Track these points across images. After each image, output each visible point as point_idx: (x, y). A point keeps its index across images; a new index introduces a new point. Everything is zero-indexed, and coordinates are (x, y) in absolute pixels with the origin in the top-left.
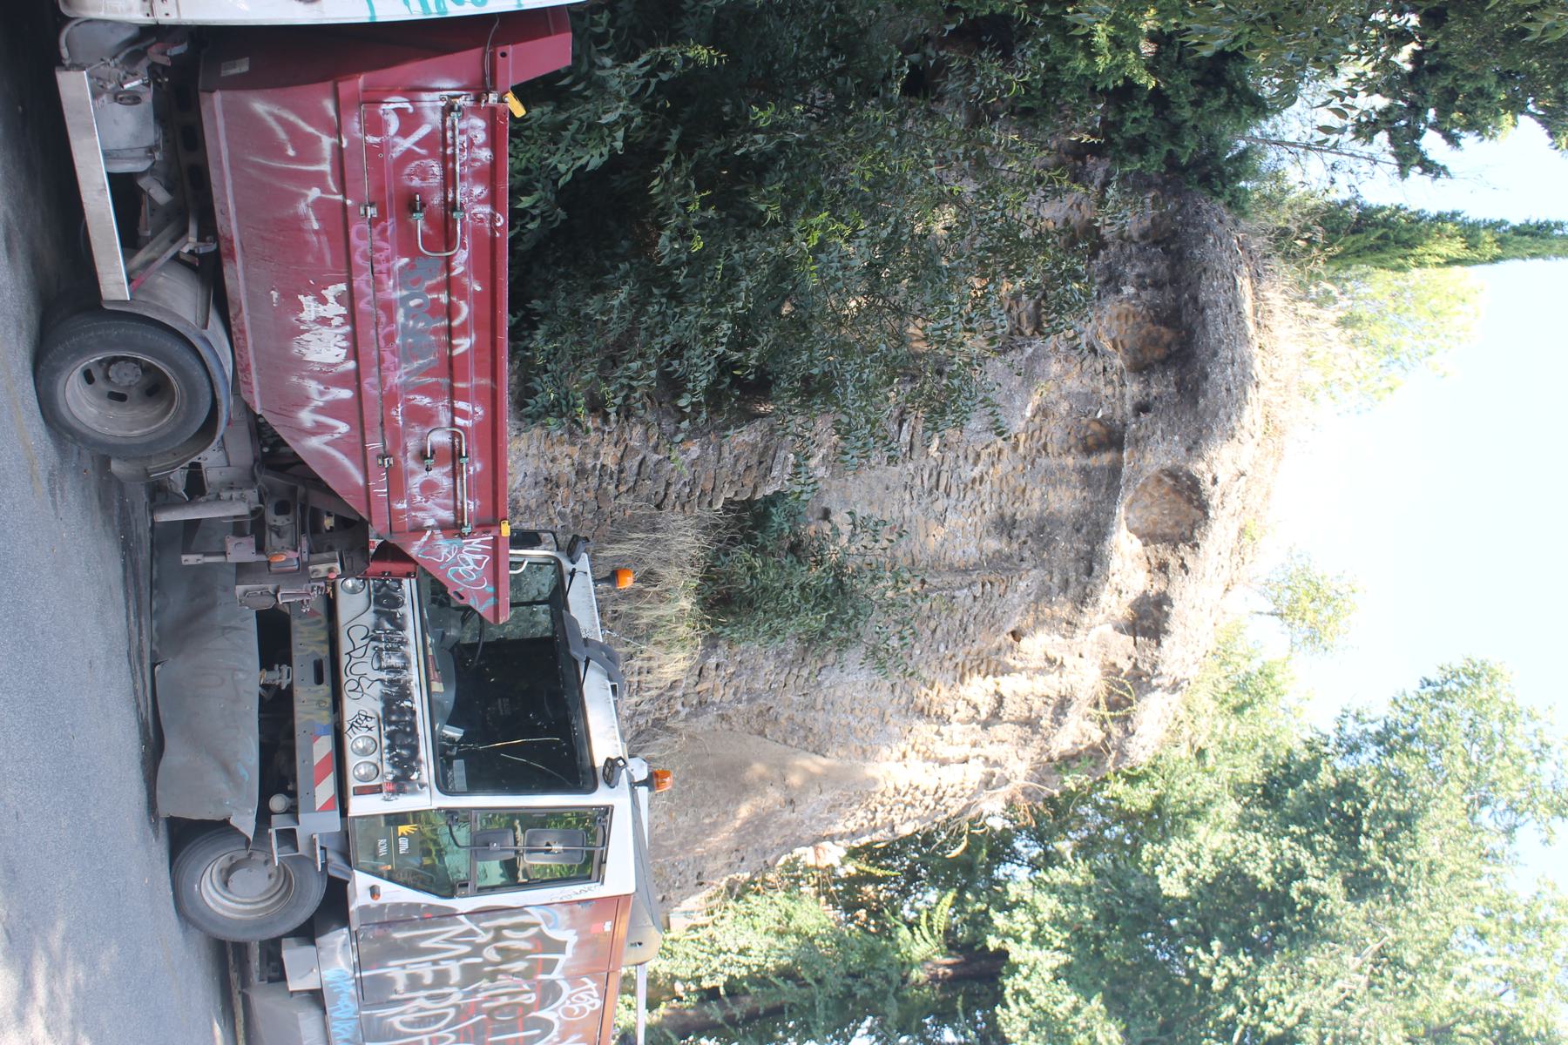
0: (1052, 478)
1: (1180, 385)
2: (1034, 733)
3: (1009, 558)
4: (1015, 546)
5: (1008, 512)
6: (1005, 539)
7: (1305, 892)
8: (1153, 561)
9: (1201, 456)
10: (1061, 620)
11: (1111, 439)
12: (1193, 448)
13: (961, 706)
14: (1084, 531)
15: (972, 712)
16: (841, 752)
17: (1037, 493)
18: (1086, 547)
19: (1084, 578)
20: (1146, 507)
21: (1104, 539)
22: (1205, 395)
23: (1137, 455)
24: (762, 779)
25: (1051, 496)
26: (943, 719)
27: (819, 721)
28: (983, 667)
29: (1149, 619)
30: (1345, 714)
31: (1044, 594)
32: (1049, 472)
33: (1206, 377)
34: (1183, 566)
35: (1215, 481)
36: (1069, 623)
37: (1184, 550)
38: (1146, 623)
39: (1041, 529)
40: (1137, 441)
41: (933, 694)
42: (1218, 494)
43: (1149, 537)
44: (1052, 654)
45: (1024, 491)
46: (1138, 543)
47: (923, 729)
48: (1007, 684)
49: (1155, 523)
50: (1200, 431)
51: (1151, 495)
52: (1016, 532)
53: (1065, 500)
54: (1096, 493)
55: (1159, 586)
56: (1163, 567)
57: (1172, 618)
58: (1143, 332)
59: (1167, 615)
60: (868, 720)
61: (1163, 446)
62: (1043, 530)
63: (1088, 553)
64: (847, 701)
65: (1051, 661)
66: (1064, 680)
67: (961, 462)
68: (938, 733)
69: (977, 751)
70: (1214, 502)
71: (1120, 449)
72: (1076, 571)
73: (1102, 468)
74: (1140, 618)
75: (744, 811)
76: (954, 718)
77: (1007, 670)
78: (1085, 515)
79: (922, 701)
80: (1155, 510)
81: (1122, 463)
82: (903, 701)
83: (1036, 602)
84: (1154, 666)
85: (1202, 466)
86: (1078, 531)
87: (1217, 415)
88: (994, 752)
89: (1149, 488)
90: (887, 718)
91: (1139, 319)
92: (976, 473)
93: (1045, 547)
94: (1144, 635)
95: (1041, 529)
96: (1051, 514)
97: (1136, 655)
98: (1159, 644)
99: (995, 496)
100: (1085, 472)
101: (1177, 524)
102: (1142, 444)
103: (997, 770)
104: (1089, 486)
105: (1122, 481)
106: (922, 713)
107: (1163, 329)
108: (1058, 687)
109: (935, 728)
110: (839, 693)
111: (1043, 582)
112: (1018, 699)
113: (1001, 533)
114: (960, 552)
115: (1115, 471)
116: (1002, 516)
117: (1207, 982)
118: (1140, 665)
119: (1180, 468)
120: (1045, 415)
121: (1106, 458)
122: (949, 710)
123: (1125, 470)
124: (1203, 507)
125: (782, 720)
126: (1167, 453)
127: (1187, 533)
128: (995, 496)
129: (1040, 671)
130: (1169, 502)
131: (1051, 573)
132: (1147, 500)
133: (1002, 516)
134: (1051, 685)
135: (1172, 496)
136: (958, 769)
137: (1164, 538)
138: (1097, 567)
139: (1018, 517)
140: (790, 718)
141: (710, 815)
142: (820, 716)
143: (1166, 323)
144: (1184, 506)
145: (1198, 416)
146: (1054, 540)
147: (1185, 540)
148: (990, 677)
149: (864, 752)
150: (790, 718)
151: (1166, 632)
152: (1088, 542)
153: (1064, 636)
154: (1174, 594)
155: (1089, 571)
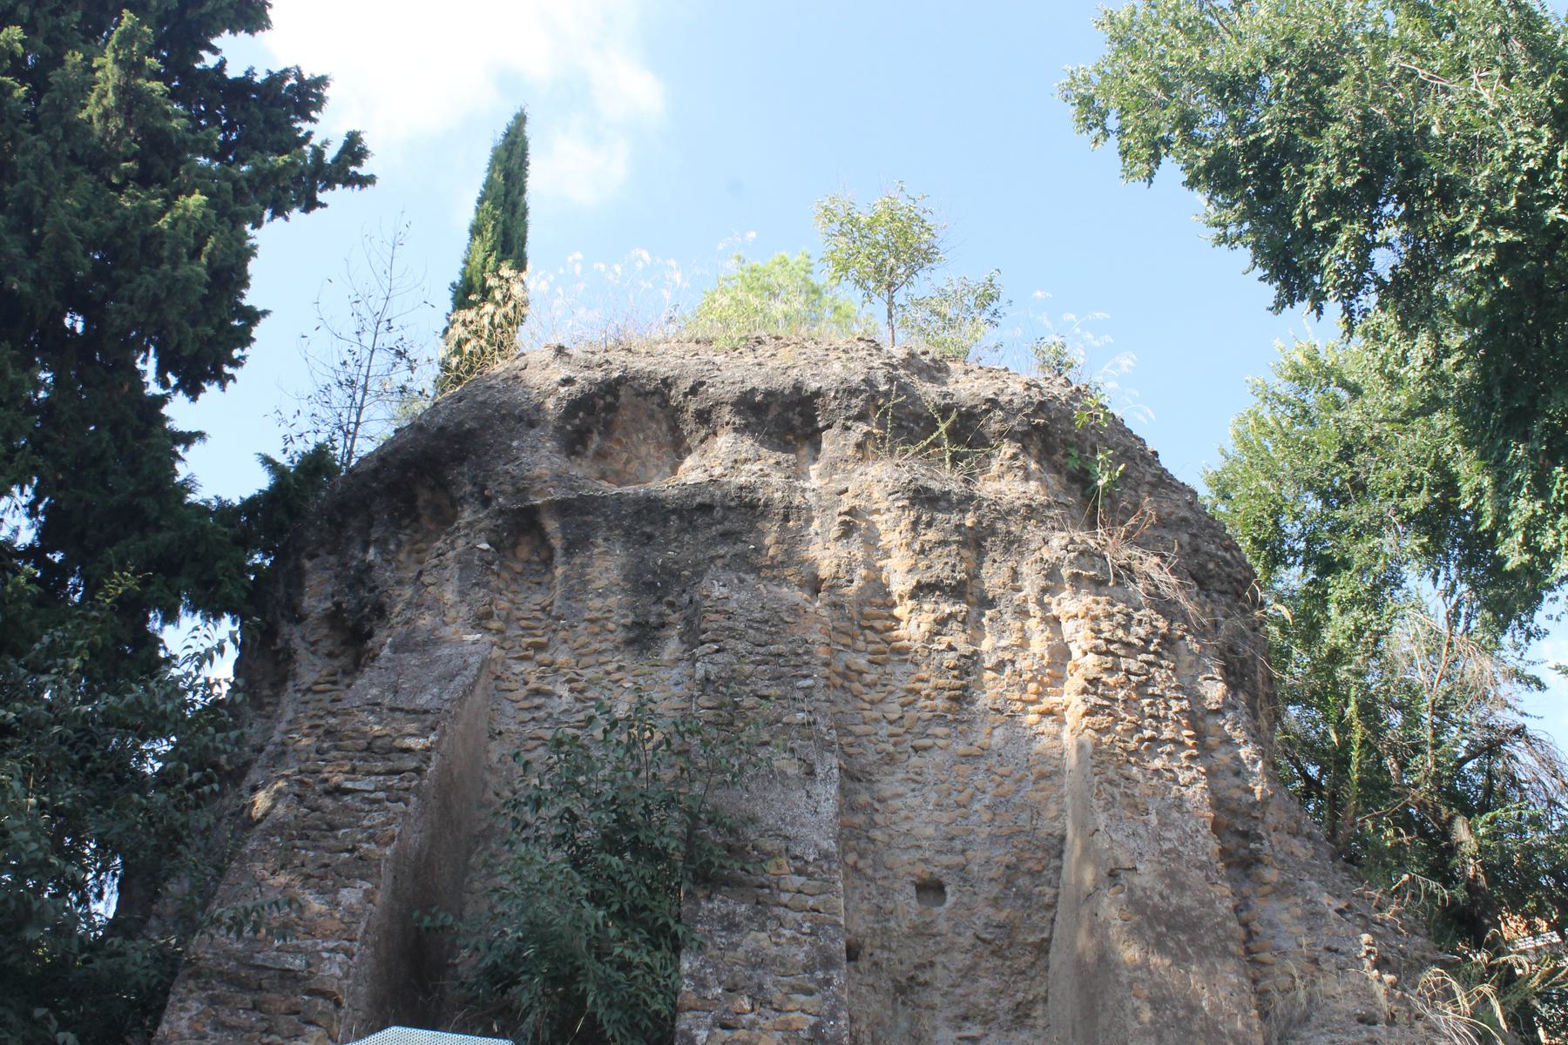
0: (578, 588)
1: (460, 459)
2: (994, 533)
3: (688, 621)
4: (674, 617)
5: (621, 635)
6: (664, 633)
7: (1344, 171)
8: (703, 433)
9: (539, 408)
10: (783, 529)
11: (522, 524)
12: (529, 418)
13: (941, 643)
14: (648, 529)
15: (954, 625)
16: (1052, 810)
17: (598, 603)
18: (674, 521)
19: (718, 513)
20: (643, 464)
21: (656, 500)
22: (461, 424)
23: (538, 486)
24: (1091, 932)
25: (600, 584)
26: (969, 665)
27: (986, 857)
28: (878, 624)
29: (787, 419)
30: (1223, 239)
31: (748, 564)
32: (569, 595)
33: (442, 429)
34: (694, 391)
35: (568, 381)
36: (786, 518)
37: (676, 395)
38: (797, 421)
39: (650, 586)
40: (519, 491)
41: (926, 689)
42: (587, 373)
43: (679, 449)
44: (835, 531)
45: (592, 621)
46: (689, 461)
47: (992, 688)
48: (899, 582)
49: (659, 446)
50: (503, 417)
51: (628, 462)
52: (653, 619)
53: (607, 565)
54: (595, 527)
55: (726, 414)
56: (703, 417)
57: (774, 385)
58: (432, 527)
59: (769, 394)
60: (979, 779)
61: (526, 457)
62: (650, 584)
63: (681, 518)
64: (945, 817)
65: (847, 530)
66: (883, 506)
67: (542, 714)
68: (999, 667)
69: (1032, 608)
70: (598, 375)
71: (533, 511)
72: (709, 526)
73: (563, 527)
74: (792, 429)
75: (1131, 953)
76: (965, 649)
77: (878, 589)
78: (628, 533)
79: (940, 703)
80: (643, 450)
81: (550, 503)
82: (941, 731)
83: (756, 569)
84: (852, 392)
85: (550, 404)
86: (650, 537)
87: (484, 403)
88: (1031, 582)
89: (618, 466)
90: (974, 750)
91: (418, 536)
92: (563, 691)
93: (675, 575)
94: (814, 419)
95: (650, 586)
96: (626, 578)
97: (840, 421)
98: (818, 394)
99: (602, 659)
100: (569, 550)
101: (651, 417)
102: (523, 484)
103: (1066, 572)
104: (587, 537)
105: (572, 495)
106: (962, 697)
107: (420, 503)
108: (895, 513)
109: (989, 675)
110: (930, 831)
111: (725, 567)
112: (922, 565)
113: (654, 639)
114: (676, 690)
115: (563, 509)
116: (629, 643)
117: (1505, 251)
118: (855, 412)
119: (558, 429)
120: (489, 615)
121: (551, 525)
122: (950, 659)
123: (558, 495)
124: (611, 388)
125: (1002, 916)
126: (535, 449)
127: (656, 399)
128: (602, 659)
129: (871, 540)
130: (627, 435)
131: (712, 559)
132: (635, 465)
133: (629, 643)
134: (892, 527)
135: (617, 434)
136: (1068, 627)
137: (675, 429)
138: (699, 499)
139: (628, 621)
140: (995, 903)
141: (1136, 1012)
142: (977, 855)
143: (411, 500)
144: (625, 415)
145: (486, 424)
146: (663, 566)
147: (665, 401)
148: (897, 612)
149: (1043, 776)
150: (995, 903)
151: (797, 388)
152: (666, 520)
153: (809, 521)
154: (732, 392)
155: (706, 508)
